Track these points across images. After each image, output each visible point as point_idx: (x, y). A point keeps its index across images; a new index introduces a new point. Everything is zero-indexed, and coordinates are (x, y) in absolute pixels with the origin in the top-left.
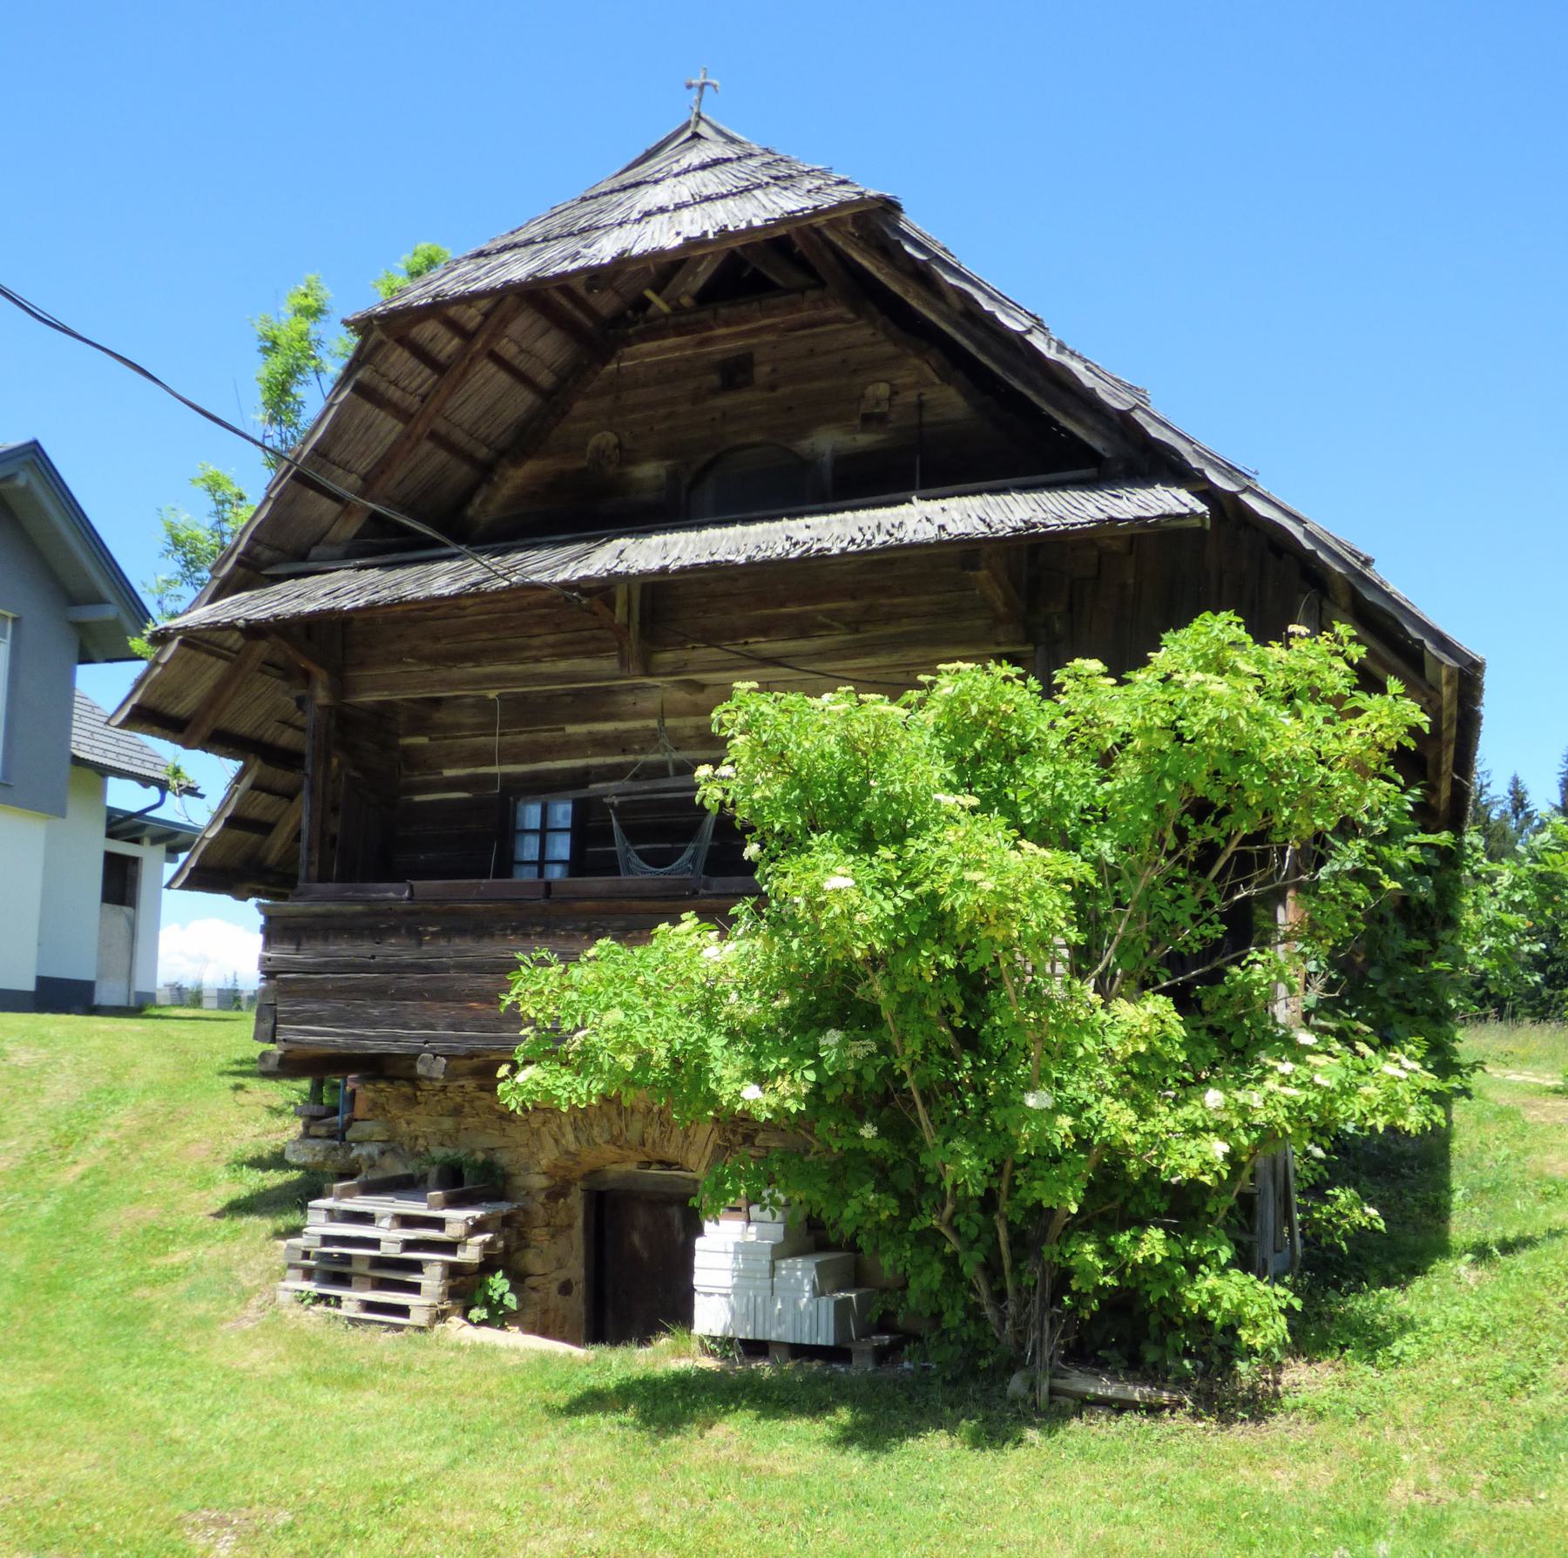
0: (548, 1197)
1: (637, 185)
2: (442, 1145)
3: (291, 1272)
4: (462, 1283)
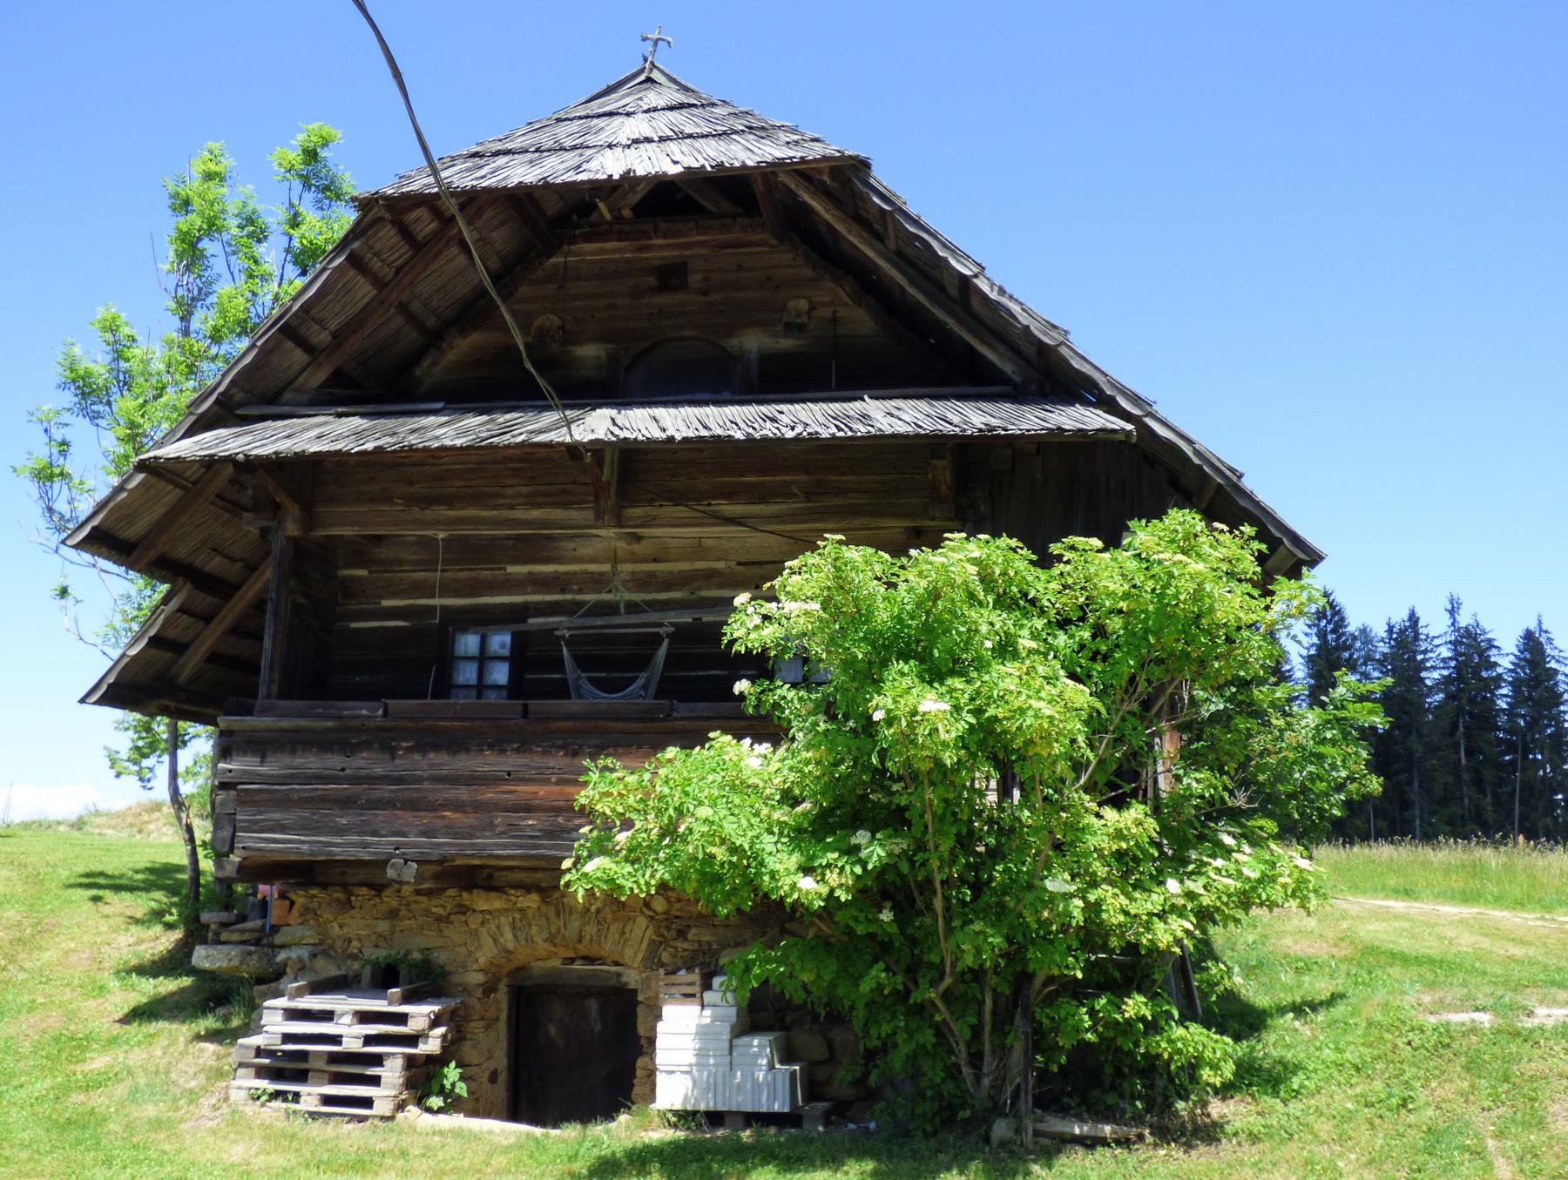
0: (484, 992)
1: (611, 114)
2: (376, 946)
3: (241, 1071)
4: (415, 1075)
